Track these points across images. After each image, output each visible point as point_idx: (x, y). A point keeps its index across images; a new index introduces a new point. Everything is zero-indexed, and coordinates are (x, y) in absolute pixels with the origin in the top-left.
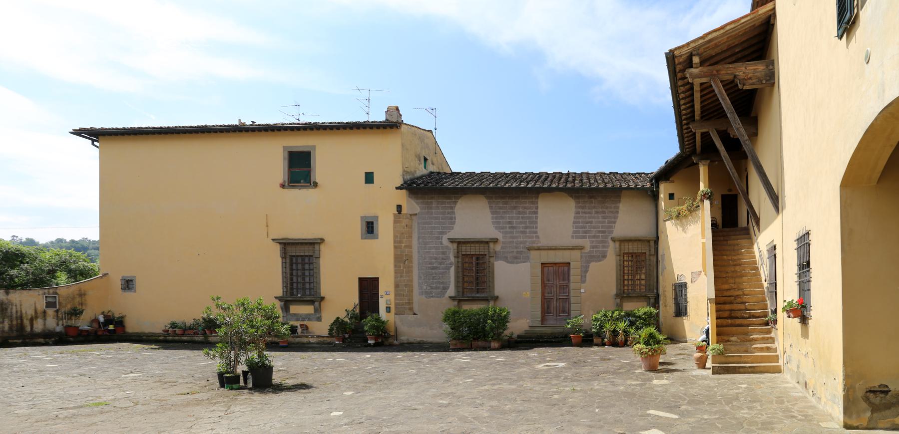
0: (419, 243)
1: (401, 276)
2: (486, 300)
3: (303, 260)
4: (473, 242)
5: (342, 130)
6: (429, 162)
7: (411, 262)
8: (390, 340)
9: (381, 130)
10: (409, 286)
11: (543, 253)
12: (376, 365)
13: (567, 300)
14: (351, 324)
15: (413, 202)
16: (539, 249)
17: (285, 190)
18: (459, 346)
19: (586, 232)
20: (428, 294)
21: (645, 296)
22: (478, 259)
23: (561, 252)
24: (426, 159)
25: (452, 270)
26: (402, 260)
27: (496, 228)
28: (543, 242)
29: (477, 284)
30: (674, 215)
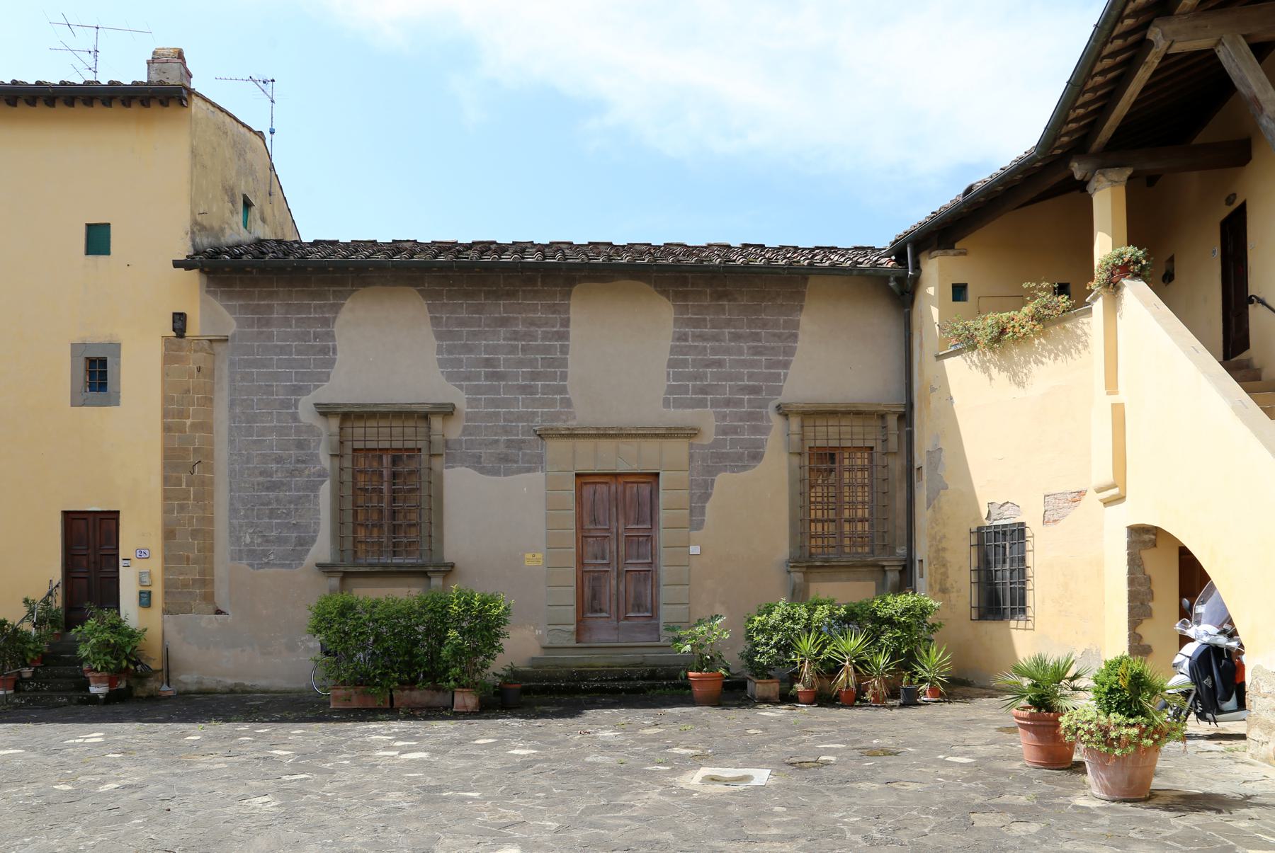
0: (233, 418)
1: (182, 508)
2: (422, 573)
4: (385, 415)
5: (22, 108)
6: (255, 211)
7: (210, 469)
8: (152, 685)
9: (136, 109)
10: (204, 533)
11: (584, 446)
12: (132, 773)
13: (649, 574)
14: (40, 638)
15: (217, 305)
16: (572, 435)
18: (355, 704)
19: (703, 391)
20: (256, 557)
21: (875, 565)
22: (395, 461)
23: (634, 443)
24: (247, 204)
25: (325, 491)
26: (183, 466)
27: (450, 377)
28: (584, 415)
29: (395, 529)
30: (982, 338)
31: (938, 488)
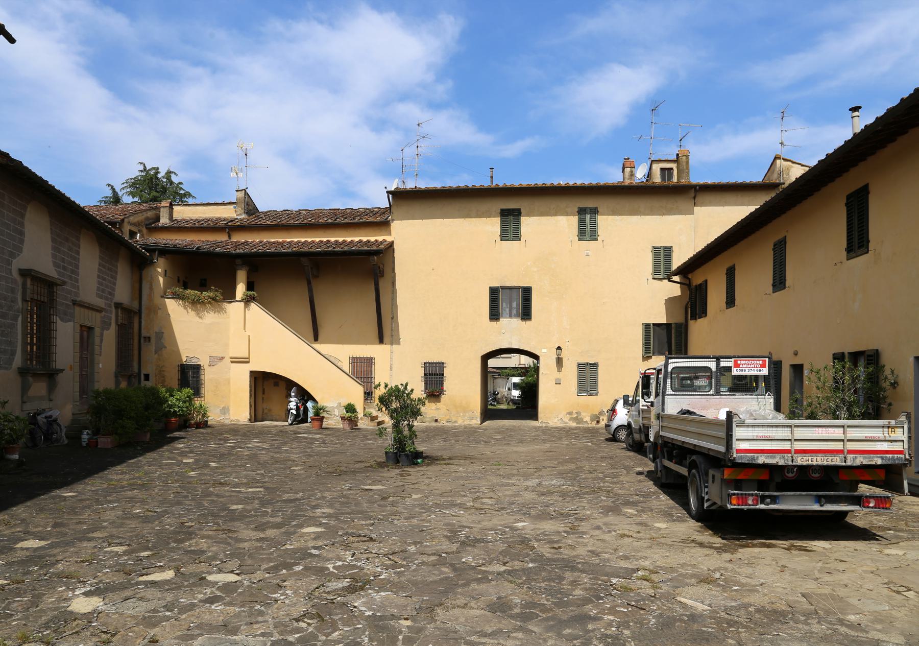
31: (160, 348)
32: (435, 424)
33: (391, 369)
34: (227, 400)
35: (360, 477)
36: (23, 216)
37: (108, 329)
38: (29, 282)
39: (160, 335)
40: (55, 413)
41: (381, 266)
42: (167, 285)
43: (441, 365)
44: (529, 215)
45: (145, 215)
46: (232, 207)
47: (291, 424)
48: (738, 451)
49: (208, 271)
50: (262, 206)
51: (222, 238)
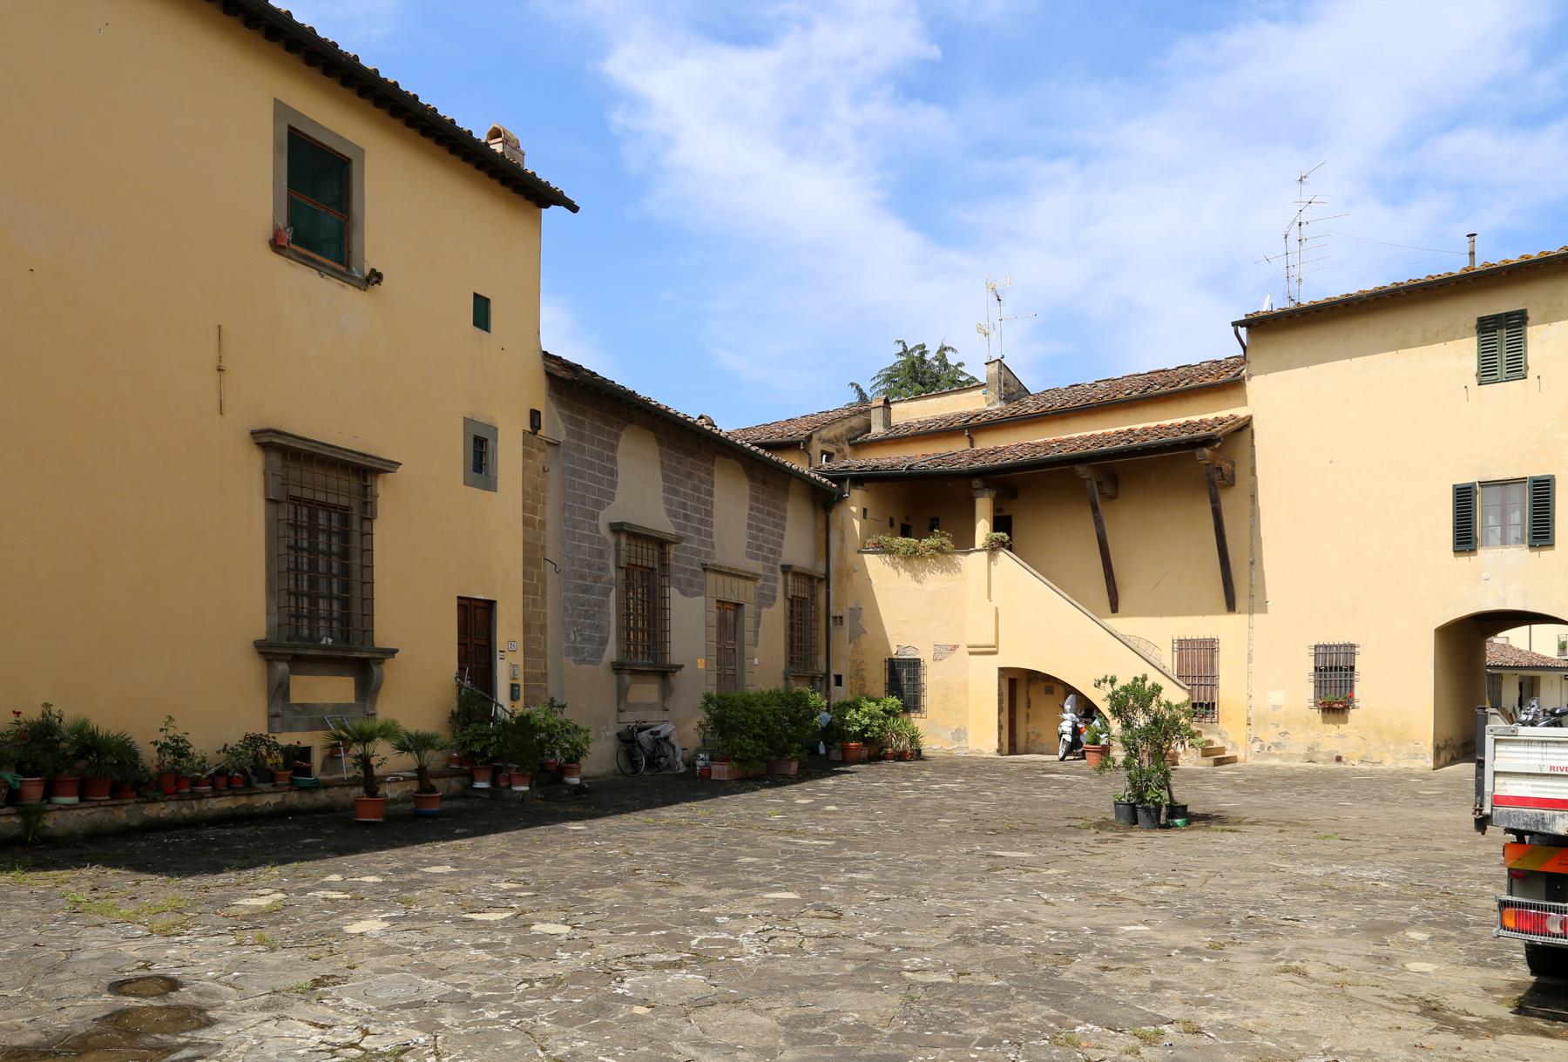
3: (313, 517)
17: (278, 260)
20: (576, 651)
25: (613, 594)
31: (857, 633)
32: (1334, 766)
33: (1250, 660)
34: (960, 717)
35: (995, 841)
36: (614, 448)
37: (770, 606)
38: (623, 540)
39: (856, 613)
40: (666, 729)
41: (1226, 466)
42: (867, 533)
43: (1350, 650)
44: (1547, 319)
45: (847, 424)
46: (980, 392)
47: (1062, 759)
48: (1498, 801)
49: (924, 508)
50: (1034, 384)
51: (959, 446)
